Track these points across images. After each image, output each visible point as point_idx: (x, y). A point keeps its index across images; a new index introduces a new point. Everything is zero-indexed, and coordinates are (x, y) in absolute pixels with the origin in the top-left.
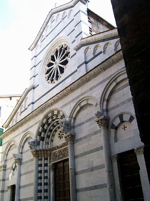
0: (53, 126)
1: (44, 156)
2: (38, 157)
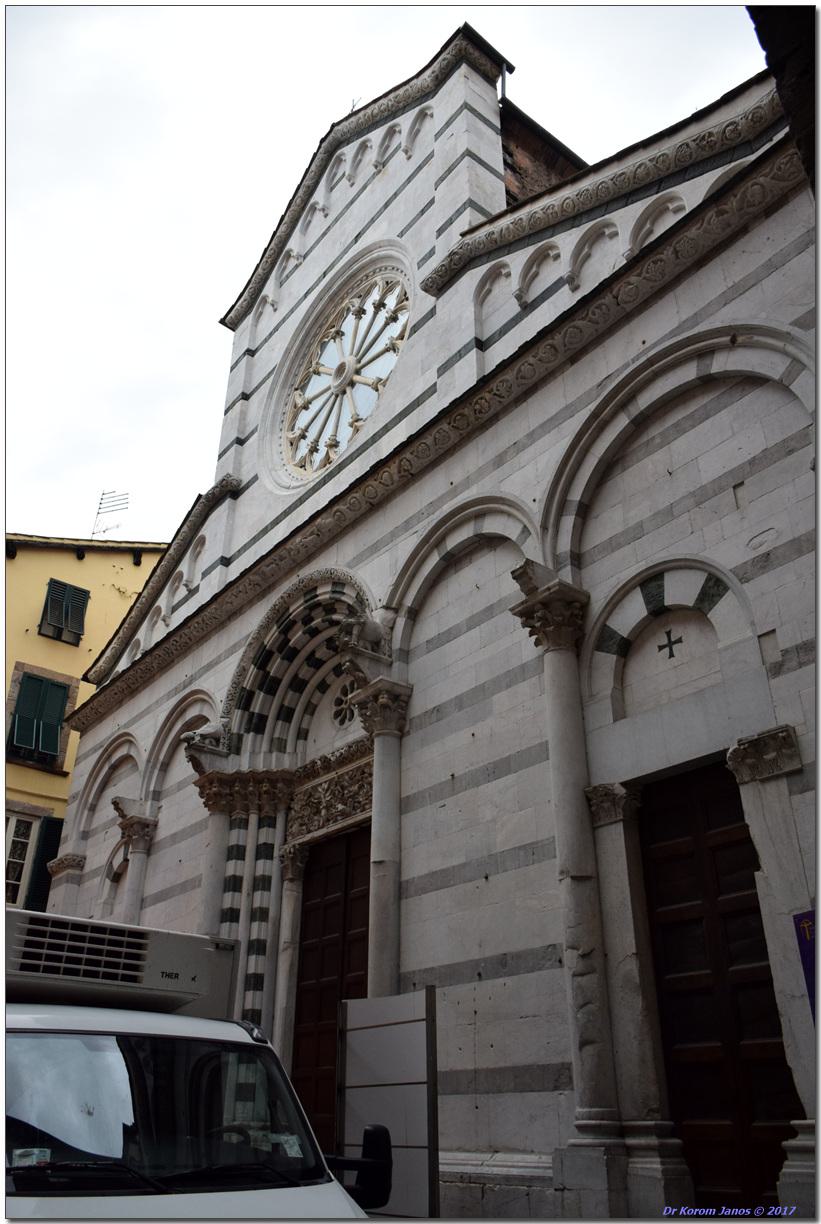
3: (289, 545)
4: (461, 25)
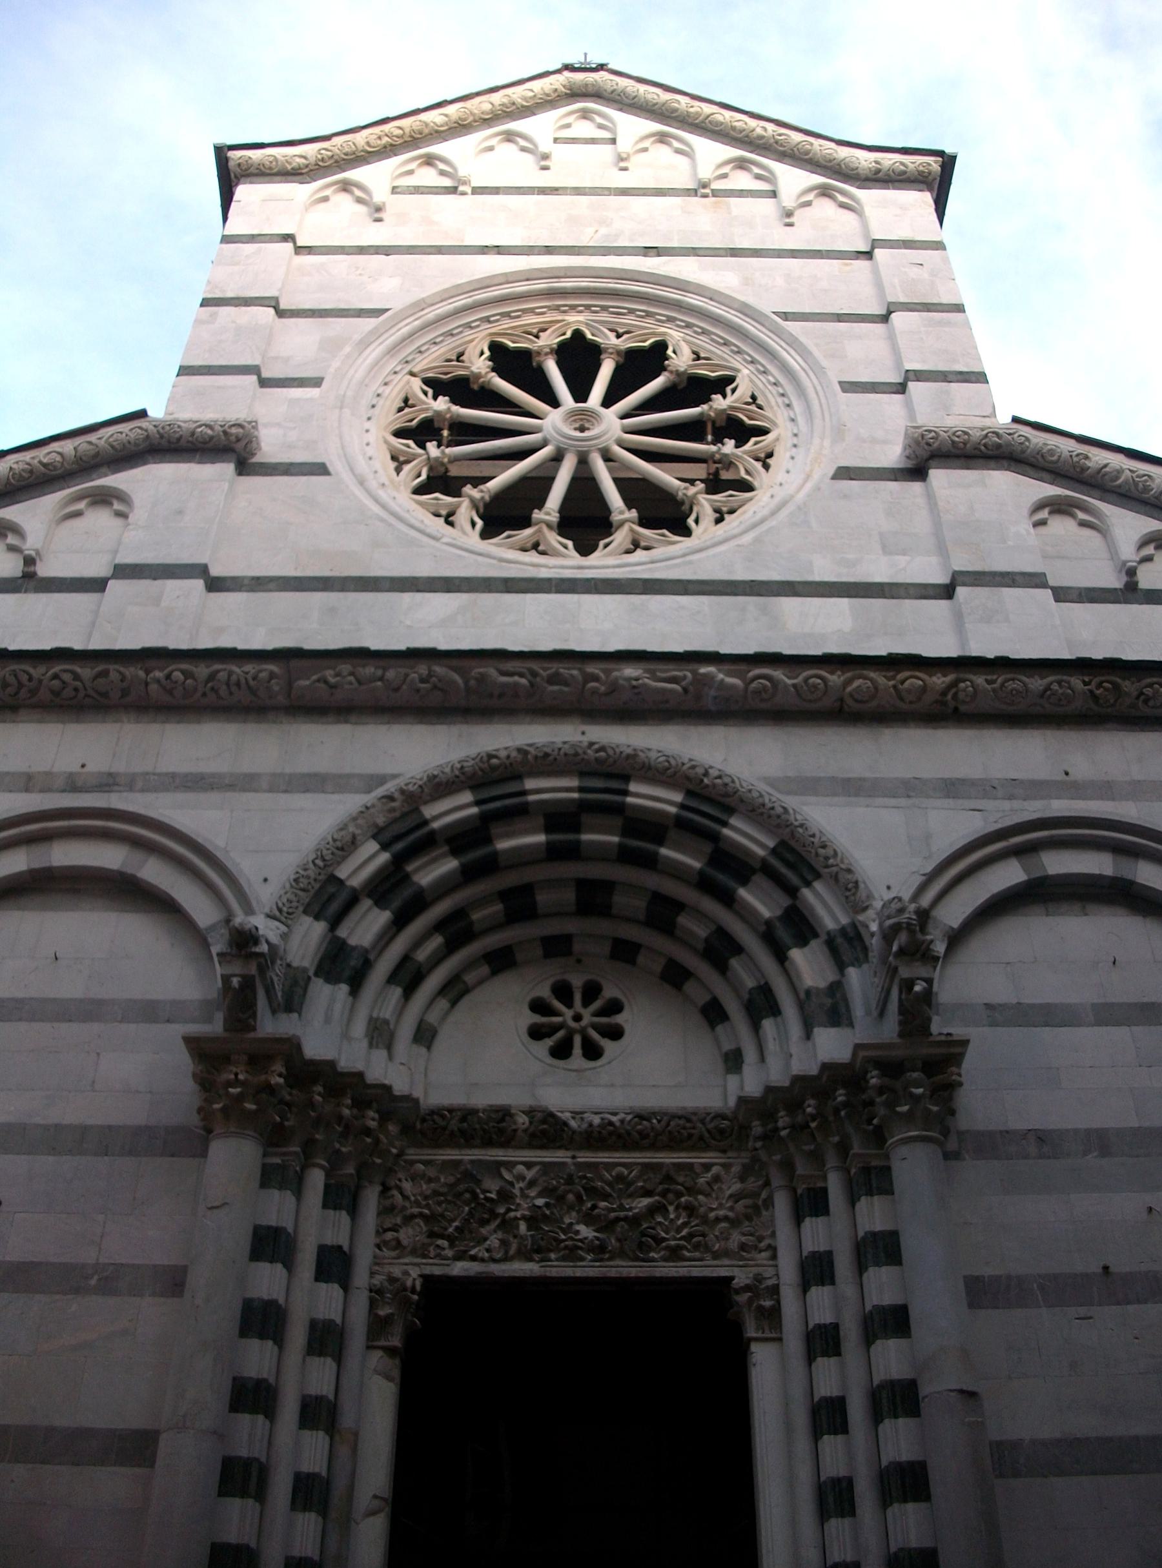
4: (949, 150)
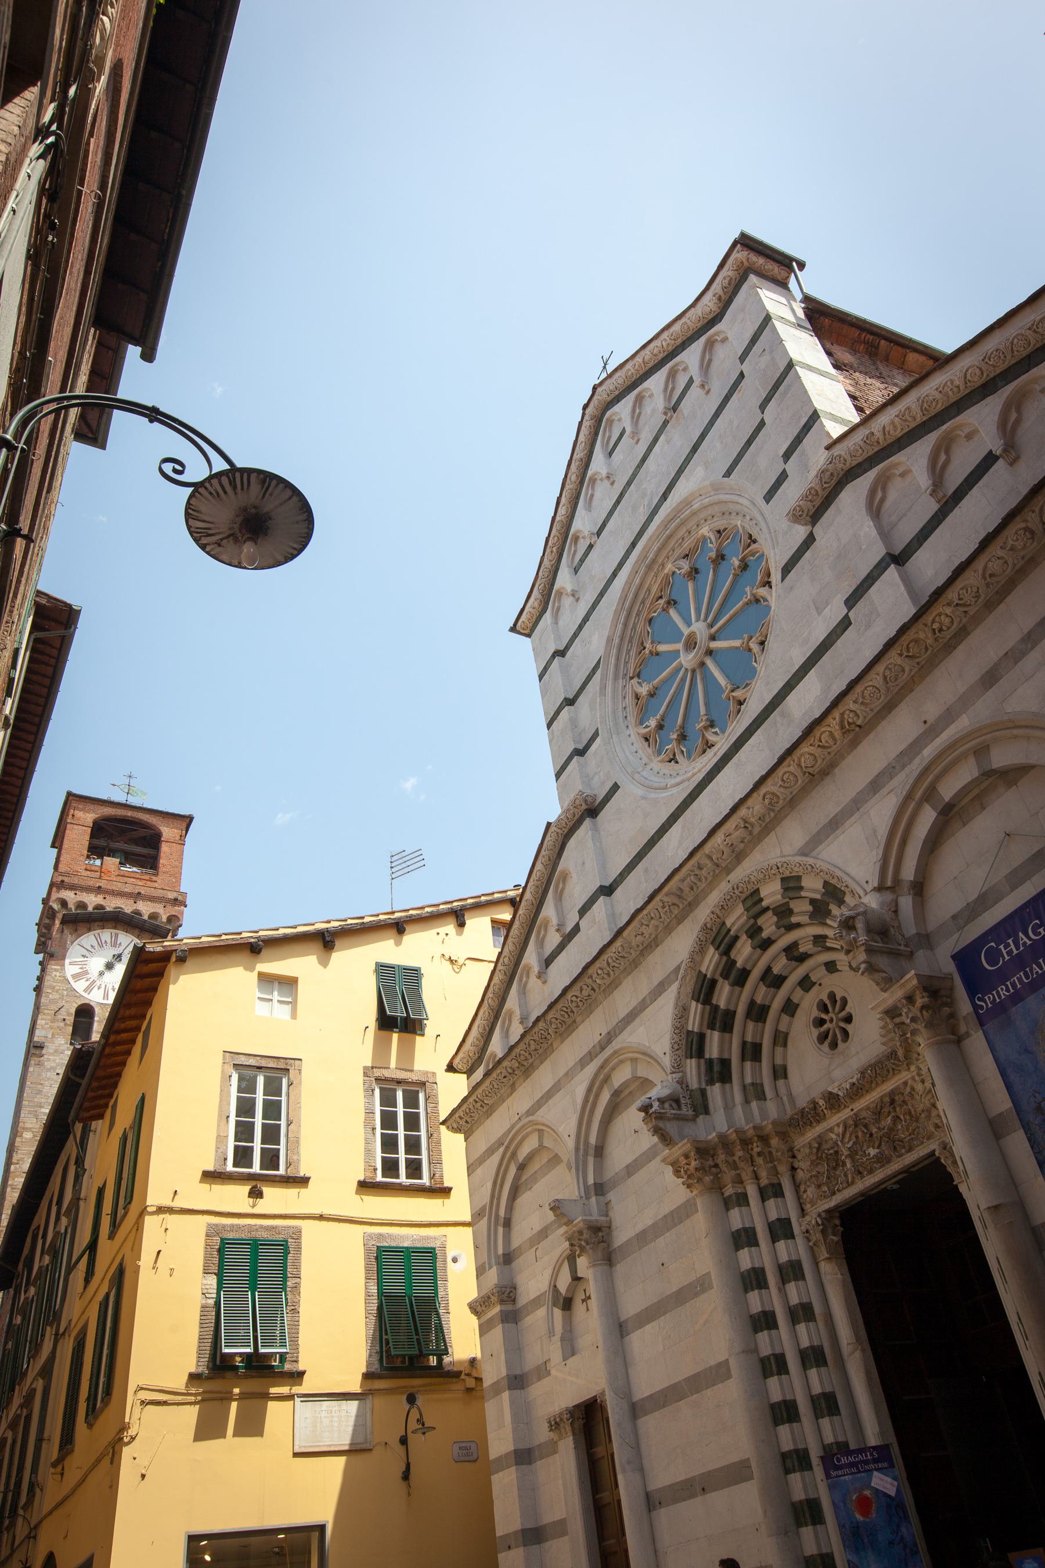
0: (769, 980)
1: (756, 1177)
2: (717, 1187)
3: (707, 848)
4: (737, 235)
